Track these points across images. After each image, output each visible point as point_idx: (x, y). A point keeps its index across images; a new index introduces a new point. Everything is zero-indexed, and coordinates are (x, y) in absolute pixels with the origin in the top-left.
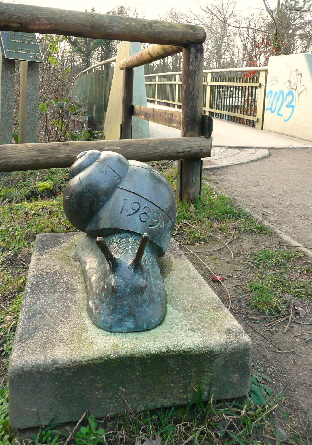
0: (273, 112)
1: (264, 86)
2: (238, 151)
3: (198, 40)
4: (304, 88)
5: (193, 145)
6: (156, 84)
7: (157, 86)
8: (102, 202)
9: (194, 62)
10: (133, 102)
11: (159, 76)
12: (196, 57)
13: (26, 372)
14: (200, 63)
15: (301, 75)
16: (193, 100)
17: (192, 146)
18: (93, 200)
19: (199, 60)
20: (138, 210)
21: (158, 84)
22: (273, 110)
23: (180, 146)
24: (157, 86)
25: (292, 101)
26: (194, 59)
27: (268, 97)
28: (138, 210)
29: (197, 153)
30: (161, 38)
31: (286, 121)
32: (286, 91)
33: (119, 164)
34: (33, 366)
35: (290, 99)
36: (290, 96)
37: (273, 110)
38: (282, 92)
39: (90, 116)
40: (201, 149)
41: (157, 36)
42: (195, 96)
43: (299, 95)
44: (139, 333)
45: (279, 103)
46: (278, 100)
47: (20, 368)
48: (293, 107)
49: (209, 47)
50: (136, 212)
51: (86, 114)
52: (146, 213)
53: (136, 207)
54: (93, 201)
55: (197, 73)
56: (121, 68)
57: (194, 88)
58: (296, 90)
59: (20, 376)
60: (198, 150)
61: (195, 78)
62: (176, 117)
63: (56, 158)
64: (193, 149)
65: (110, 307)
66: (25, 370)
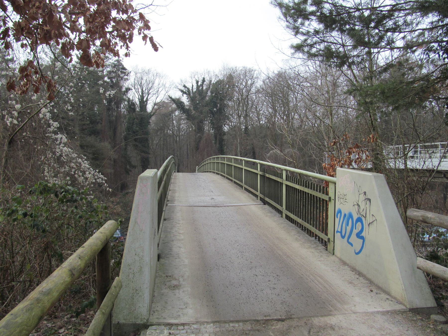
0: (343, 237)
1: (334, 201)
4: (374, 219)
10: (146, 18)
15: (370, 200)
22: (343, 235)
25: (362, 231)
27: (337, 217)
31: (357, 254)
32: (355, 217)
33: (170, 274)
35: (360, 228)
36: (359, 224)
37: (343, 235)
38: (351, 216)
43: (369, 225)
44: (172, 181)
45: (349, 228)
46: (348, 224)
48: (362, 238)
49: (409, 54)
51: (410, 23)
58: (365, 218)
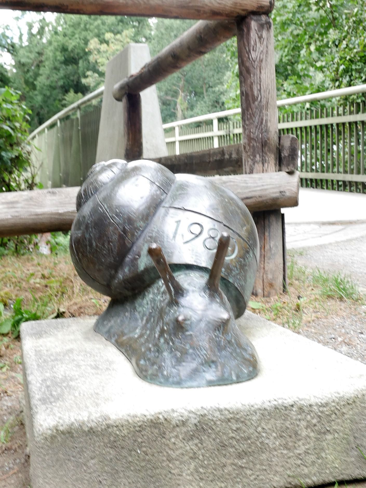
2: (340, 227)
3: (262, 7)
5: (267, 185)
6: (174, 143)
7: (177, 144)
8: (139, 230)
9: (258, 45)
11: (181, 127)
12: (260, 37)
13: (63, 433)
14: (267, 47)
16: (261, 112)
17: (265, 187)
18: (124, 228)
19: (265, 43)
20: (200, 233)
21: (181, 142)
23: (247, 187)
24: (177, 144)
26: (257, 40)
28: (200, 233)
29: (275, 200)
30: (198, 7)
34: (72, 424)
39: (37, 251)
40: (281, 192)
41: (191, 5)
42: (264, 102)
47: (53, 427)
50: (197, 236)
52: (213, 238)
53: (196, 229)
54: (124, 231)
55: (263, 64)
56: (117, 96)
57: (260, 90)
59: (53, 437)
60: (276, 193)
61: (260, 72)
62: (231, 155)
63: (37, 215)
64: (268, 192)
65: (176, 355)
66: (61, 428)
